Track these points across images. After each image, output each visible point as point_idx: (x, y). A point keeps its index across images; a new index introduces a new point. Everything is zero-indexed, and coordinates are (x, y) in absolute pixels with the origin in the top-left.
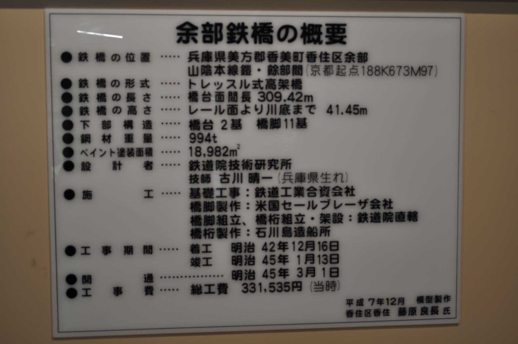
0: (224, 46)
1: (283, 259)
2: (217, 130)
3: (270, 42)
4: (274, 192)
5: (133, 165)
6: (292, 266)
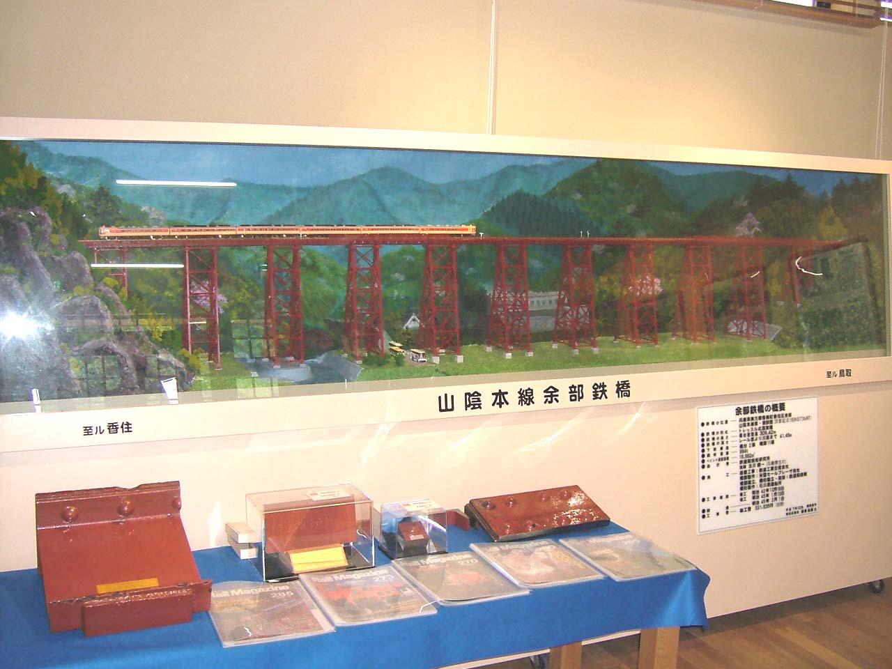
0: (750, 415)
1: (768, 495)
2: (748, 448)
3: (763, 412)
4: (765, 470)
5: (723, 463)
6: (770, 498)
